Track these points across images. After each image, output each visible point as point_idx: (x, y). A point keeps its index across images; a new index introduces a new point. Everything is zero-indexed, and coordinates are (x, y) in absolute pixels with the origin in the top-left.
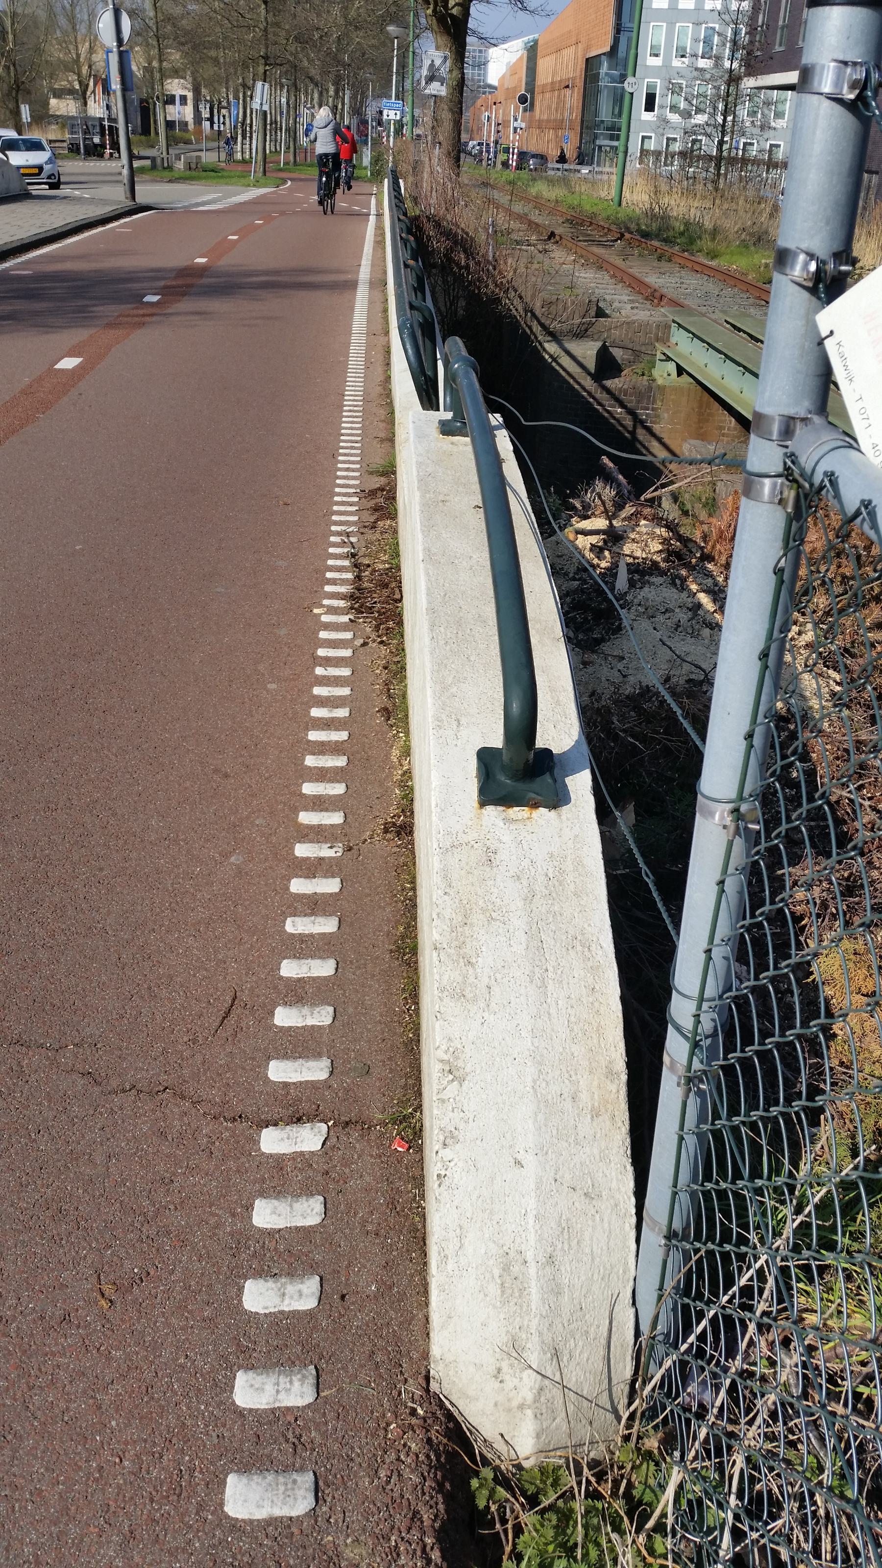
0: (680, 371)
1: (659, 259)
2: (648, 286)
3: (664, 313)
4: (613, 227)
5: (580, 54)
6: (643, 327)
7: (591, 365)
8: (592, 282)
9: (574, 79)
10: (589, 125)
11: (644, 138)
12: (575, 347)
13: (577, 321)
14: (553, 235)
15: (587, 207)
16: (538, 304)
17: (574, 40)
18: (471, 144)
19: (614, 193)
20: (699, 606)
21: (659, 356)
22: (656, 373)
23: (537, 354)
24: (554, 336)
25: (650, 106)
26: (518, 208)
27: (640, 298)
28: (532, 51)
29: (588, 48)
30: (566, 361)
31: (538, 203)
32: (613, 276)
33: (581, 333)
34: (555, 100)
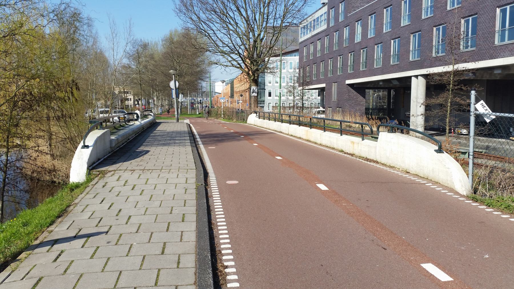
25: (270, 95)
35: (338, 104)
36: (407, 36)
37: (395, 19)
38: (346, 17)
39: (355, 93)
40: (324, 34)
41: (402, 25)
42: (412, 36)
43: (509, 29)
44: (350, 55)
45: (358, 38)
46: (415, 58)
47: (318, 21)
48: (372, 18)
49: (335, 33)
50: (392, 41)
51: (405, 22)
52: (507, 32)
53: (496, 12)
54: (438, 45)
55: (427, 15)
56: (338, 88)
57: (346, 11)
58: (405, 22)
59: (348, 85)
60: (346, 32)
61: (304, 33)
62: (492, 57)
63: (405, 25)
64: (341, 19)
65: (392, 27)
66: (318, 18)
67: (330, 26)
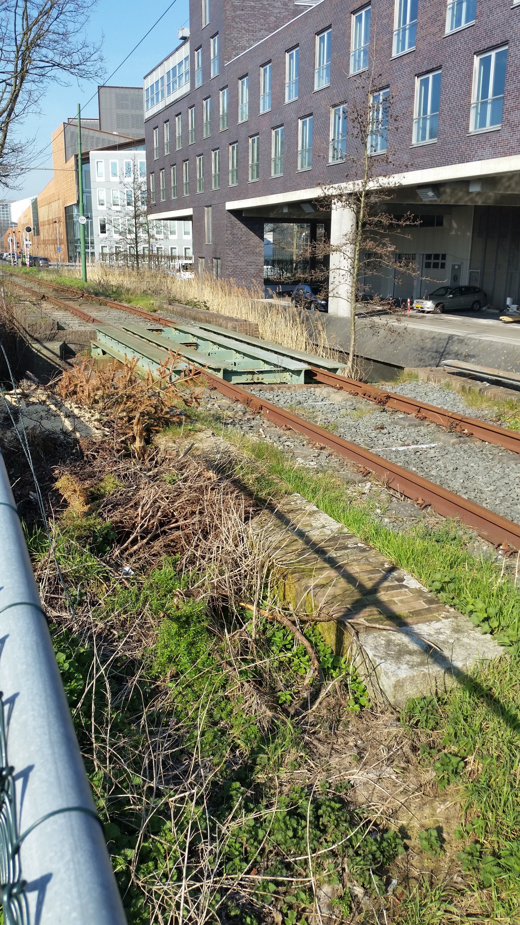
0: (104, 353)
1: (101, 305)
2: (87, 316)
3: (90, 327)
4: (79, 292)
5: (61, 205)
6: (82, 333)
7: (58, 352)
8: (59, 315)
9: (59, 218)
10: (71, 242)
11: (186, 249)
12: (48, 345)
13: (48, 332)
14: (44, 296)
15: (68, 283)
16: (27, 326)
17: (57, 198)
18: (5, 254)
19: (82, 276)
20: (50, 409)
21: (92, 346)
22: (92, 354)
23: (29, 350)
24: (37, 340)
25: (103, 229)
26: (28, 285)
27: (84, 321)
28: (35, 205)
29: (64, 203)
30: (45, 351)
31: (40, 283)
32: (73, 313)
33: (52, 338)
34: (51, 229)
35: (215, 251)
36: (323, 111)
37: (305, 76)
38: (221, 68)
39: (245, 229)
40: (185, 105)
41: (316, 89)
42: (417, 81)
43: (494, 100)
44: (231, 148)
45: (243, 114)
46: (424, 138)
47: (174, 75)
48: (322, 40)
49: (204, 102)
50: (300, 122)
51: (321, 82)
52: (489, 107)
53: (472, 63)
54: (425, 119)
55: (403, 49)
56: (213, 217)
57: (223, 56)
58: (321, 82)
59: (233, 212)
60: (223, 98)
61: (152, 99)
62: (463, 159)
63: (322, 87)
64: (214, 72)
65: (300, 93)
66: (174, 69)
67: (197, 87)
